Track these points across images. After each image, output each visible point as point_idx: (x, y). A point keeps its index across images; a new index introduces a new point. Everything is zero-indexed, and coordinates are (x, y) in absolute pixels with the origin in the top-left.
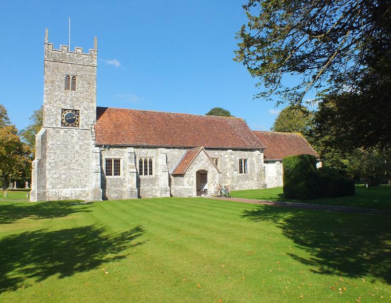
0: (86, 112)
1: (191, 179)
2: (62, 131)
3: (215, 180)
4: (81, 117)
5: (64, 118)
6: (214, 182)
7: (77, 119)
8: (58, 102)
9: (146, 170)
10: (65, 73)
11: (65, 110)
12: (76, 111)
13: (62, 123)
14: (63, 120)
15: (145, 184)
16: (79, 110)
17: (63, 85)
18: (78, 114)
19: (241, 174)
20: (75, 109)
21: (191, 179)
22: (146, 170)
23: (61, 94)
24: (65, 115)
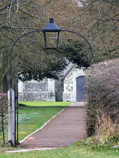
1: (71, 85)
15: (34, 89)
21: (71, 85)
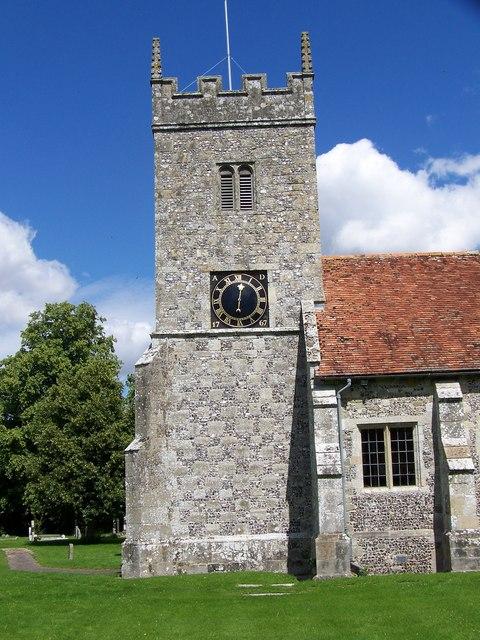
0: (288, 274)
2: (214, 344)
4: (273, 292)
5: (219, 301)
7: (257, 290)
8: (199, 253)
10: (215, 158)
12: (256, 273)
13: (214, 317)
14: (217, 307)
16: (265, 272)
17: (214, 196)
18: (265, 283)
23: (208, 227)
24: (221, 291)
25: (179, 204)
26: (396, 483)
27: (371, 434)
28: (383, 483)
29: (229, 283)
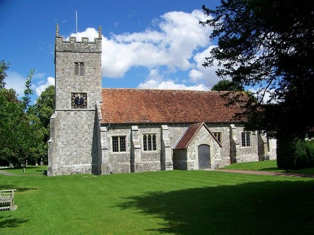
1: (193, 153)
2: (72, 113)
3: (217, 154)
5: (74, 101)
6: (216, 156)
9: (150, 146)
11: (74, 94)
16: (86, 93)
19: (244, 147)
20: (83, 92)
22: (150, 146)
23: (71, 80)
25: (63, 73)
26: (248, 145)
27: (115, 139)
28: (151, 150)
29: (76, 96)
